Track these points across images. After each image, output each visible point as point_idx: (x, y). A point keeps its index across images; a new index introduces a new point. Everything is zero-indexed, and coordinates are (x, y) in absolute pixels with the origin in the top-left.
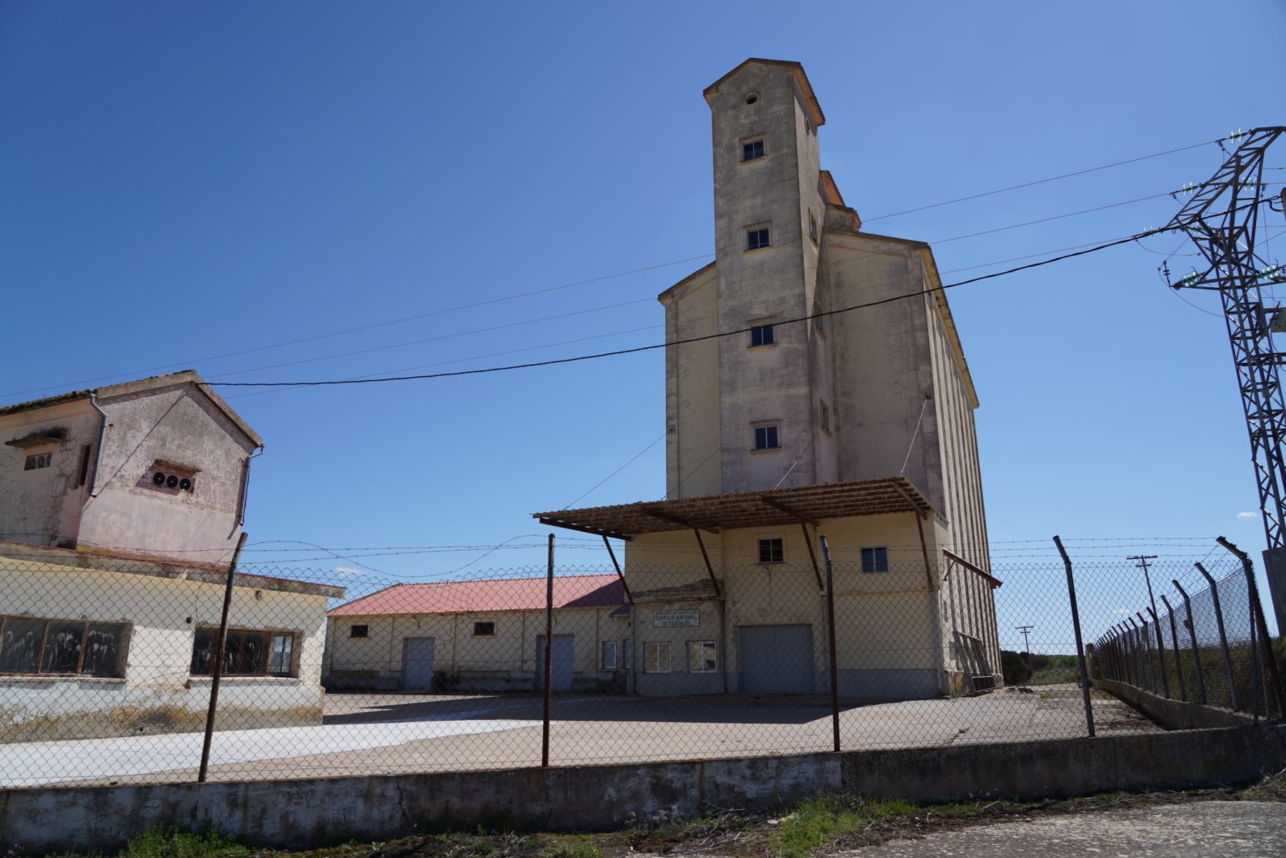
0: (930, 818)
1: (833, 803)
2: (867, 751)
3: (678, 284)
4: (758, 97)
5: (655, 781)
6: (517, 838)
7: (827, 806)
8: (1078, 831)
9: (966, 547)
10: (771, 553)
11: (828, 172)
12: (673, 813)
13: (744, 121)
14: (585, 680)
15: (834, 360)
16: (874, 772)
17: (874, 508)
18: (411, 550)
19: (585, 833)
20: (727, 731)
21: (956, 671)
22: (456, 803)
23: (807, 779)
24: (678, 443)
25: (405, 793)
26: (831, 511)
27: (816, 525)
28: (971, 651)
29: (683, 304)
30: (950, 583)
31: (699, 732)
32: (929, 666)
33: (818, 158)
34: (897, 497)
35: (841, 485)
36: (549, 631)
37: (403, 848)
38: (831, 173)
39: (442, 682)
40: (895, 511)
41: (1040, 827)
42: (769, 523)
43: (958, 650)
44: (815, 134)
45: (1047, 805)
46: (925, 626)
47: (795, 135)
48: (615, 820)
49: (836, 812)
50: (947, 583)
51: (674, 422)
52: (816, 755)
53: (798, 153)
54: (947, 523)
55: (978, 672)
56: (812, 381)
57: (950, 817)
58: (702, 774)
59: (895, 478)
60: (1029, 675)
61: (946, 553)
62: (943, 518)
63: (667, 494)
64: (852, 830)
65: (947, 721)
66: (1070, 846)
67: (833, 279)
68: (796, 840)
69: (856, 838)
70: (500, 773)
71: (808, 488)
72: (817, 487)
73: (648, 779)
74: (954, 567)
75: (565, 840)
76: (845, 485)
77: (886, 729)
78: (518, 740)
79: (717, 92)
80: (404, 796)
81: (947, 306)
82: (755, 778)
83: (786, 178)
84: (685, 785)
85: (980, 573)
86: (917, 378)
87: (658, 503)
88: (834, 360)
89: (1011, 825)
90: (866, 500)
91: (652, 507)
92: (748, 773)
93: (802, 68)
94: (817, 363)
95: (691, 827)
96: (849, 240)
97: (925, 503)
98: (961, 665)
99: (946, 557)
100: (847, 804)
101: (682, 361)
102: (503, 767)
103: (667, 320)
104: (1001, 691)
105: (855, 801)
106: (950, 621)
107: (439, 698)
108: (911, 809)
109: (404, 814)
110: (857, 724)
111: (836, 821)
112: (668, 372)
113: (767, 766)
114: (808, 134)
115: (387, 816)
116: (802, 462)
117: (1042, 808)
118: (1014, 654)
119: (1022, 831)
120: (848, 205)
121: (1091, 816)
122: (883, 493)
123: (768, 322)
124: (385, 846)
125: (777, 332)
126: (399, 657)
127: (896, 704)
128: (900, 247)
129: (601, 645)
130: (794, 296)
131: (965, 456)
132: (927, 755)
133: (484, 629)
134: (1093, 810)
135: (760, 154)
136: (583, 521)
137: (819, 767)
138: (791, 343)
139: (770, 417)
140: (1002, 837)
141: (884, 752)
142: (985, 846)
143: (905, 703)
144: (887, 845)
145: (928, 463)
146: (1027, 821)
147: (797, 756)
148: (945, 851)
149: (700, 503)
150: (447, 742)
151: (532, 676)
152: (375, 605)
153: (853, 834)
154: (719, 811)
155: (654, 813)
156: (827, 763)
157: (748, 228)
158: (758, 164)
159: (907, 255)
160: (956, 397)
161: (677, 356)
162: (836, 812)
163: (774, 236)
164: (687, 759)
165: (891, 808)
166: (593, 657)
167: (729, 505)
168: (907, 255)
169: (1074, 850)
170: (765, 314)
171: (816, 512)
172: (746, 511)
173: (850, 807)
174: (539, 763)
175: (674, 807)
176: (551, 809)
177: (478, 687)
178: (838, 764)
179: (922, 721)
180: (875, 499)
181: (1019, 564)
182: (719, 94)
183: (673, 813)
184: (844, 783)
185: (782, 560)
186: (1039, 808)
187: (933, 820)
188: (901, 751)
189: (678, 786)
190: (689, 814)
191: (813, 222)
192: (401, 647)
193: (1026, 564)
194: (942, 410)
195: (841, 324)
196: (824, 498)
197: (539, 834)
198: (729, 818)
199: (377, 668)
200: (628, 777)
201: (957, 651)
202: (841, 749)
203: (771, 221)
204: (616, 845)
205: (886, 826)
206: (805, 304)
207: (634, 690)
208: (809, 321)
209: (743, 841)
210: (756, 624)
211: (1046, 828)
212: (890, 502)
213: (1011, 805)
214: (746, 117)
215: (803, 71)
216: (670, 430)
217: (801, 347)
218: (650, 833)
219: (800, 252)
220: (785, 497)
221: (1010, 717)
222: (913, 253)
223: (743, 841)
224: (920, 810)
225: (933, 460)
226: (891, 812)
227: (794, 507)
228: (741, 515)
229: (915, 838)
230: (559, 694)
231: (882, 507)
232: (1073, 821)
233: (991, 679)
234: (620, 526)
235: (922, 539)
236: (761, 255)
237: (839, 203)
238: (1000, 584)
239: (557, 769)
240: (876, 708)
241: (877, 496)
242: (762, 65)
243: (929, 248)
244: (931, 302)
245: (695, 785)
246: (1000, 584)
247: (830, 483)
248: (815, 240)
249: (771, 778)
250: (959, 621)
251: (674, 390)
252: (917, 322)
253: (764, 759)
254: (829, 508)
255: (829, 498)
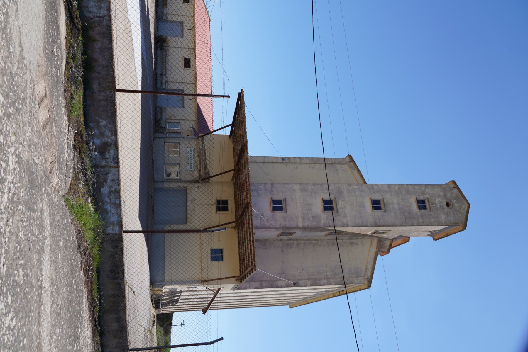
0: (91, 273)
1: (98, 228)
2: (123, 246)
3: (356, 165)
4: (449, 208)
5: (109, 144)
6: (81, 75)
7: (97, 226)
8: (84, 341)
9: (222, 299)
10: (222, 206)
11: (409, 241)
12: (93, 152)
13: (437, 200)
14: (161, 113)
15: (315, 240)
16: (113, 249)
17: (242, 256)
18: (223, 25)
19: (83, 109)
20: (136, 182)
21: (163, 291)
22: (98, 45)
23: (110, 217)
24: (277, 163)
25: (102, 19)
26: (241, 235)
27: (235, 228)
28: (173, 299)
29: (346, 167)
30: (205, 290)
31: (135, 168)
32: (166, 278)
33: (417, 236)
34: (247, 267)
35: (253, 241)
36: (185, 95)
37: (75, 17)
38: (408, 243)
39: (161, 41)
40: (240, 266)
41: (86, 324)
42: (236, 205)
43: (173, 293)
44: (428, 235)
45: (97, 328)
46: (184, 277)
47: (429, 226)
48: (90, 124)
49: (94, 230)
50: (205, 288)
51: (287, 161)
52: (121, 222)
53: (419, 227)
54: (234, 290)
55: (163, 302)
56: (305, 229)
57: (91, 283)
58: (113, 167)
59: (256, 266)
60: (161, 326)
61: (219, 289)
62: (237, 288)
63: (252, 156)
64: (85, 237)
65: (140, 285)
66: (77, 336)
67: (355, 241)
68: (80, 210)
69: (81, 238)
70: (113, 68)
71: (252, 224)
72: (252, 229)
73: (110, 141)
74: (212, 292)
75: (80, 99)
76: (253, 242)
77: (136, 257)
78: (132, 80)
79: (453, 187)
80: (101, 19)
81: (339, 295)
82: (110, 192)
83: (407, 220)
84: (107, 158)
85: (210, 304)
86: (304, 279)
87: (247, 152)
88: (315, 240)
89: (88, 310)
90: (246, 252)
91: (245, 148)
92: (113, 189)
93: (463, 230)
94: (313, 232)
95: (87, 160)
96: (374, 250)
97: (243, 280)
98: (166, 293)
99: (217, 289)
100: (98, 235)
101: (317, 166)
102: (115, 70)
103: (338, 159)
104: (153, 312)
105: (99, 239)
106: (187, 290)
107: (153, 41)
108: (95, 265)
109: (92, 18)
110: (138, 243)
111: (90, 230)
112: (312, 158)
113: (116, 198)
114: (429, 232)
115: (91, 10)
116: (266, 222)
117: (95, 325)
118: (172, 319)
119: (85, 315)
120: (391, 250)
121: (91, 347)
122: (249, 260)
123: (335, 208)
124: (75, 8)
125: (329, 213)
126: (175, 19)
127: (148, 263)
128: (369, 274)
129: (178, 121)
130: (347, 222)
131: (266, 300)
132: (121, 273)
133: (187, 63)
134: (94, 349)
135: (420, 208)
136: (239, 114)
137: (115, 223)
138: (324, 219)
139: (288, 208)
140: (82, 306)
141: (122, 253)
142: (77, 298)
143: (148, 266)
144: (78, 253)
145: (263, 282)
146: (89, 318)
147: (121, 213)
148: (75, 279)
149: (246, 172)
150: (130, 44)
151: (164, 87)
152: (200, 7)
153: (83, 237)
154: (95, 175)
155: (93, 143)
156: (117, 227)
157: (382, 200)
158: (414, 206)
159: (365, 277)
160: (295, 298)
161: (320, 163)
162: (94, 230)
163: (378, 213)
164: (120, 160)
165: (96, 256)
166: (172, 118)
167: (245, 186)
168: (365, 277)
169: (75, 338)
170: (339, 207)
171: (241, 228)
172: (242, 195)
173: (96, 236)
174: (117, 87)
175: (96, 153)
176: (95, 93)
177: (159, 59)
178: (117, 232)
179: (139, 274)
180: (246, 256)
181: (210, 320)
182: (452, 188)
183: (93, 152)
184: (108, 234)
185: (218, 211)
186: (96, 324)
187: (90, 275)
188: (123, 261)
189: (107, 155)
190: (93, 160)
191: (384, 232)
192: (179, 20)
193: (210, 324)
194: (288, 290)
195: (332, 244)
196: (247, 232)
197: (83, 86)
198: (91, 179)
199: (169, 7)
200: (111, 131)
201: (172, 292)
202: (124, 234)
203: (385, 212)
204: (78, 124)
205: (87, 253)
206: (343, 227)
207: (156, 137)
208: (333, 228)
209: (80, 185)
210: (187, 198)
211: (86, 326)
212: (244, 264)
213: (97, 312)
214: (440, 202)
215: (461, 231)
216: (283, 159)
217: (322, 224)
218: (84, 141)
219: (369, 225)
220: (248, 213)
221: (141, 314)
222: (366, 280)
223: (80, 185)
224: (95, 269)
225: (264, 285)
226: (94, 256)
227: (244, 218)
228: (240, 192)
229: (81, 266)
230: (155, 100)
231: (242, 260)
232: (89, 339)
233: (159, 308)
234: (236, 132)
235: (226, 278)
236: (369, 206)
237: (393, 246)
238: (204, 313)
239: (114, 96)
240: (146, 253)
241: (248, 257)
242: (466, 211)
243: (368, 288)
244: (341, 288)
245: (107, 164)
246: (204, 313)
247: (255, 236)
248: (374, 233)
249: (110, 200)
250: (187, 293)
251: (303, 161)
252: (332, 280)
253: (119, 197)
254: (242, 234)
255: (247, 234)
